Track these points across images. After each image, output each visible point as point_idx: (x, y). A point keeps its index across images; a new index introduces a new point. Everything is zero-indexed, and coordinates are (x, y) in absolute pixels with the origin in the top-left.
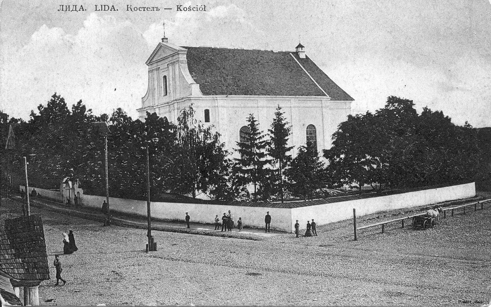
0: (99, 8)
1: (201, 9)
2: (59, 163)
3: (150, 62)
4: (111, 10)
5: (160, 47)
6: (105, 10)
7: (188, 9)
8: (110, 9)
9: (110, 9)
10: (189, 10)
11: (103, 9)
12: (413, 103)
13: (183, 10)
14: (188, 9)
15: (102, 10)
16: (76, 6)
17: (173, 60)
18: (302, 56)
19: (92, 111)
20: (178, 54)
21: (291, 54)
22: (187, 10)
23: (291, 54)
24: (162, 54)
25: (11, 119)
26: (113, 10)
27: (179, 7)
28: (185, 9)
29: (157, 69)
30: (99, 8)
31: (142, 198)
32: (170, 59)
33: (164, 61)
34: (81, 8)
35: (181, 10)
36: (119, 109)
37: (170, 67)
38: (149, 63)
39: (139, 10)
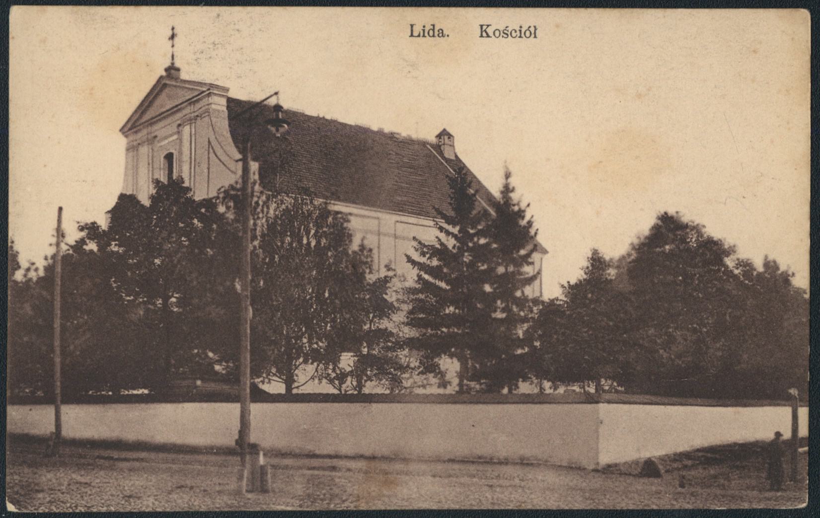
1: (528, 34)
3: (131, 127)
5: (159, 88)
7: (502, 34)
10: (503, 36)
13: (493, 37)
14: (502, 34)
17: (194, 112)
20: (209, 95)
22: (501, 36)
24: (165, 102)
25: (526, 382)
27: (484, 27)
28: (497, 33)
29: (148, 140)
31: (49, 399)
32: (187, 111)
33: (171, 118)
35: (488, 36)
36: (595, 252)
37: (186, 130)
38: (130, 129)
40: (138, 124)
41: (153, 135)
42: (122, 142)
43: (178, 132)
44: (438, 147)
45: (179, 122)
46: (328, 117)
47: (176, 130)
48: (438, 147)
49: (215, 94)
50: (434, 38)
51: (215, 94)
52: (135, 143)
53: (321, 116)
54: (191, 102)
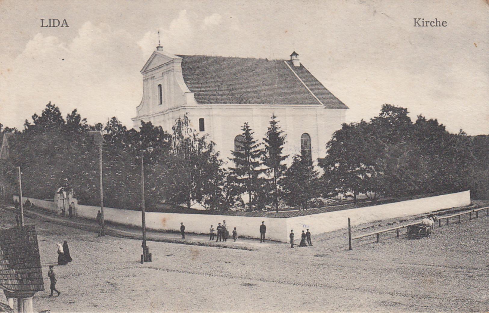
0: (46, 23)
4: (62, 26)
6: (54, 26)
16: (42, 26)
26: (65, 25)
27: (417, 20)
30: (46, 23)
34: (64, 23)
38: (144, 72)
40: (149, 69)
41: (153, 75)
42: (141, 77)
43: (163, 76)
44: (291, 62)
45: (163, 72)
46: (234, 56)
47: (161, 75)
48: (291, 62)
49: (175, 62)
50: (440, 27)
51: (175, 62)
52: (147, 78)
53: (230, 57)
54: (167, 64)
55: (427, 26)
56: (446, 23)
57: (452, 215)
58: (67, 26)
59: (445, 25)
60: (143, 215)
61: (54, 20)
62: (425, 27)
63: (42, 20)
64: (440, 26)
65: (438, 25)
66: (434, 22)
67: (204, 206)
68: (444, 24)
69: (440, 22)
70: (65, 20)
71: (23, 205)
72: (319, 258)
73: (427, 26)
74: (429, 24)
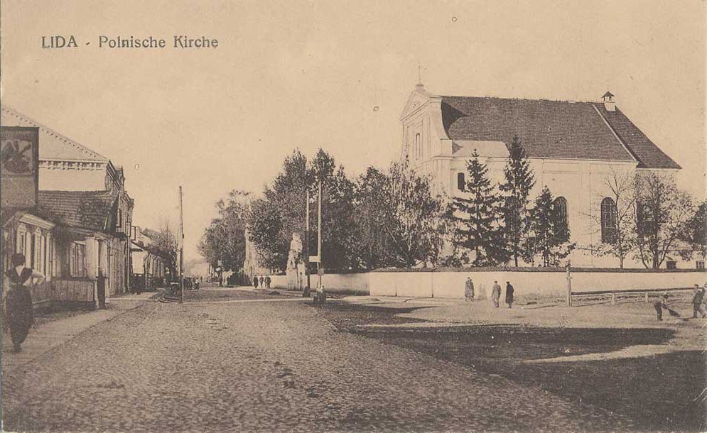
0: (48, 42)
2: (168, 273)
4: (69, 46)
6: (57, 47)
7: (141, 43)
8: (67, 44)
9: (67, 44)
11: (55, 45)
12: (40, 159)
14: (141, 43)
15: (52, 46)
18: (610, 107)
19: (231, 191)
21: (594, 106)
23: (594, 106)
26: (72, 45)
30: (48, 42)
34: (72, 41)
39: (144, 46)
55: (190, 46)
56: (164, 42)
57: (232, 287)
58: (76, 45)
59: (162, 45)
60: (622, 266)
61: (57, 38)
62: (188, 48)
63: (43, 38)
64: (156, 46)
65: (154, 45)
66: (200, 41)
67: (530, 265)
68: (215, 43)
69: (156, 41)
70: (72, 38)
71: (304, 296)
72: (531, 305)
73: (190, 46)
74: (193, 43)
